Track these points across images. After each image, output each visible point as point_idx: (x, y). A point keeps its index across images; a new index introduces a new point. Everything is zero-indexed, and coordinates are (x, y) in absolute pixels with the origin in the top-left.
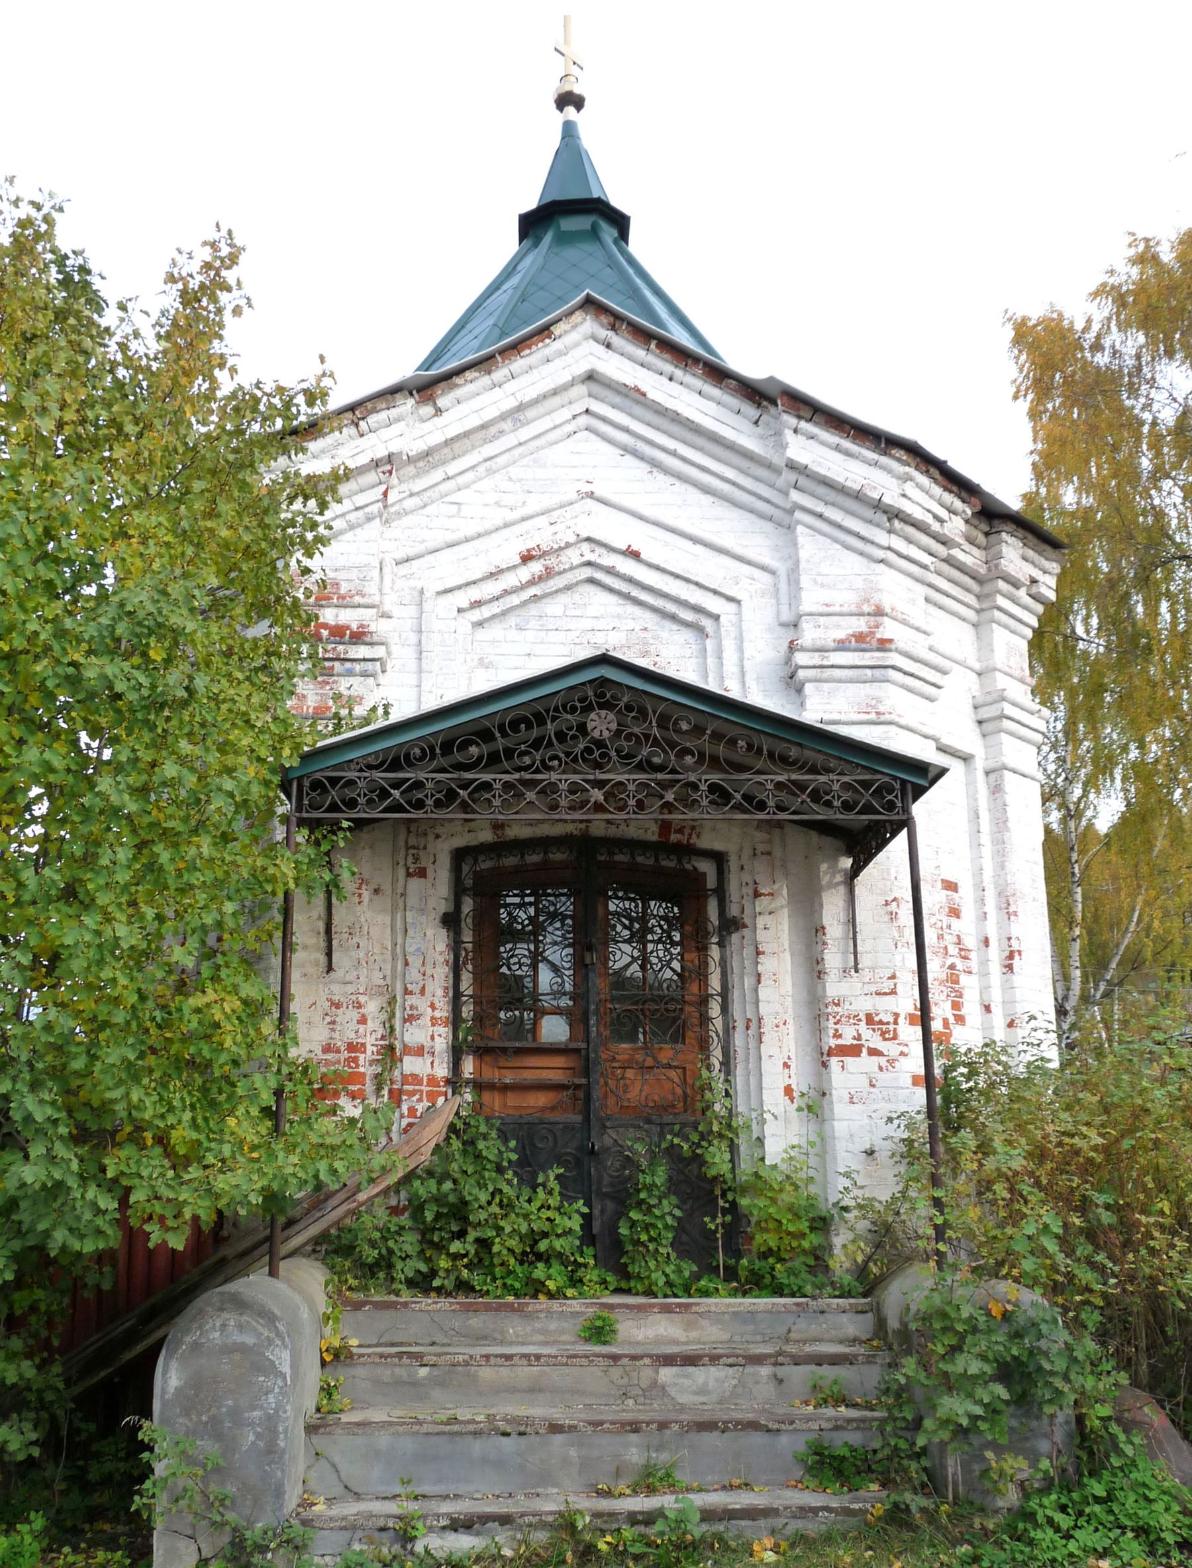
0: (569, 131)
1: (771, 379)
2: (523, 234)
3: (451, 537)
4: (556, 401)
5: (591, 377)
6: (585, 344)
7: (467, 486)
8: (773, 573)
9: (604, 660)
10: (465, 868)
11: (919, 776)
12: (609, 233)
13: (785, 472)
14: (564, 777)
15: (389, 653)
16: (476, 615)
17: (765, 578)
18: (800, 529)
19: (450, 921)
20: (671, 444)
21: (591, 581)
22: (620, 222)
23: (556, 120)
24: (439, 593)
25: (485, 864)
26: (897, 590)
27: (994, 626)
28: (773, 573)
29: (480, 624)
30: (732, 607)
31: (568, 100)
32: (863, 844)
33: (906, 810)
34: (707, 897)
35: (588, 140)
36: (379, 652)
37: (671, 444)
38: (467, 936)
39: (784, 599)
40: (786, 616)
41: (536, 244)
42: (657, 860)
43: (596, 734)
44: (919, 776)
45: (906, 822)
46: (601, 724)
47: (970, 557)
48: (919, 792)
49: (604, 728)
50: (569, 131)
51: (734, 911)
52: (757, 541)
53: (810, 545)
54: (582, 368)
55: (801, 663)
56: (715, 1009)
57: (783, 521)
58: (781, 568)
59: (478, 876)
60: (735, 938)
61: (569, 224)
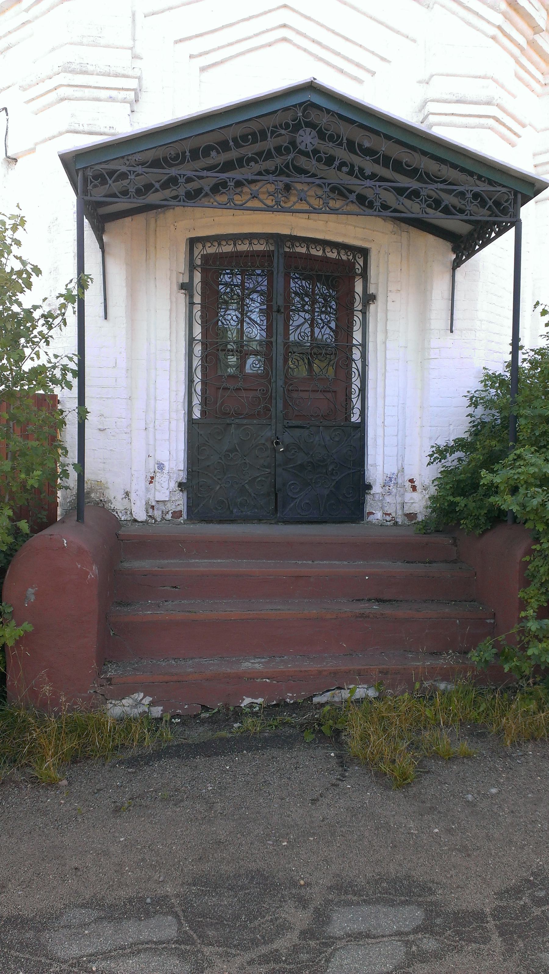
25: (211, 250)
29: (203, 69)
32: (465, 245)
33: (516, 214)
38: (197, 299)
45: (517, 223)
48: (526, 199)
59: (206, 258)
60: (372, 307)
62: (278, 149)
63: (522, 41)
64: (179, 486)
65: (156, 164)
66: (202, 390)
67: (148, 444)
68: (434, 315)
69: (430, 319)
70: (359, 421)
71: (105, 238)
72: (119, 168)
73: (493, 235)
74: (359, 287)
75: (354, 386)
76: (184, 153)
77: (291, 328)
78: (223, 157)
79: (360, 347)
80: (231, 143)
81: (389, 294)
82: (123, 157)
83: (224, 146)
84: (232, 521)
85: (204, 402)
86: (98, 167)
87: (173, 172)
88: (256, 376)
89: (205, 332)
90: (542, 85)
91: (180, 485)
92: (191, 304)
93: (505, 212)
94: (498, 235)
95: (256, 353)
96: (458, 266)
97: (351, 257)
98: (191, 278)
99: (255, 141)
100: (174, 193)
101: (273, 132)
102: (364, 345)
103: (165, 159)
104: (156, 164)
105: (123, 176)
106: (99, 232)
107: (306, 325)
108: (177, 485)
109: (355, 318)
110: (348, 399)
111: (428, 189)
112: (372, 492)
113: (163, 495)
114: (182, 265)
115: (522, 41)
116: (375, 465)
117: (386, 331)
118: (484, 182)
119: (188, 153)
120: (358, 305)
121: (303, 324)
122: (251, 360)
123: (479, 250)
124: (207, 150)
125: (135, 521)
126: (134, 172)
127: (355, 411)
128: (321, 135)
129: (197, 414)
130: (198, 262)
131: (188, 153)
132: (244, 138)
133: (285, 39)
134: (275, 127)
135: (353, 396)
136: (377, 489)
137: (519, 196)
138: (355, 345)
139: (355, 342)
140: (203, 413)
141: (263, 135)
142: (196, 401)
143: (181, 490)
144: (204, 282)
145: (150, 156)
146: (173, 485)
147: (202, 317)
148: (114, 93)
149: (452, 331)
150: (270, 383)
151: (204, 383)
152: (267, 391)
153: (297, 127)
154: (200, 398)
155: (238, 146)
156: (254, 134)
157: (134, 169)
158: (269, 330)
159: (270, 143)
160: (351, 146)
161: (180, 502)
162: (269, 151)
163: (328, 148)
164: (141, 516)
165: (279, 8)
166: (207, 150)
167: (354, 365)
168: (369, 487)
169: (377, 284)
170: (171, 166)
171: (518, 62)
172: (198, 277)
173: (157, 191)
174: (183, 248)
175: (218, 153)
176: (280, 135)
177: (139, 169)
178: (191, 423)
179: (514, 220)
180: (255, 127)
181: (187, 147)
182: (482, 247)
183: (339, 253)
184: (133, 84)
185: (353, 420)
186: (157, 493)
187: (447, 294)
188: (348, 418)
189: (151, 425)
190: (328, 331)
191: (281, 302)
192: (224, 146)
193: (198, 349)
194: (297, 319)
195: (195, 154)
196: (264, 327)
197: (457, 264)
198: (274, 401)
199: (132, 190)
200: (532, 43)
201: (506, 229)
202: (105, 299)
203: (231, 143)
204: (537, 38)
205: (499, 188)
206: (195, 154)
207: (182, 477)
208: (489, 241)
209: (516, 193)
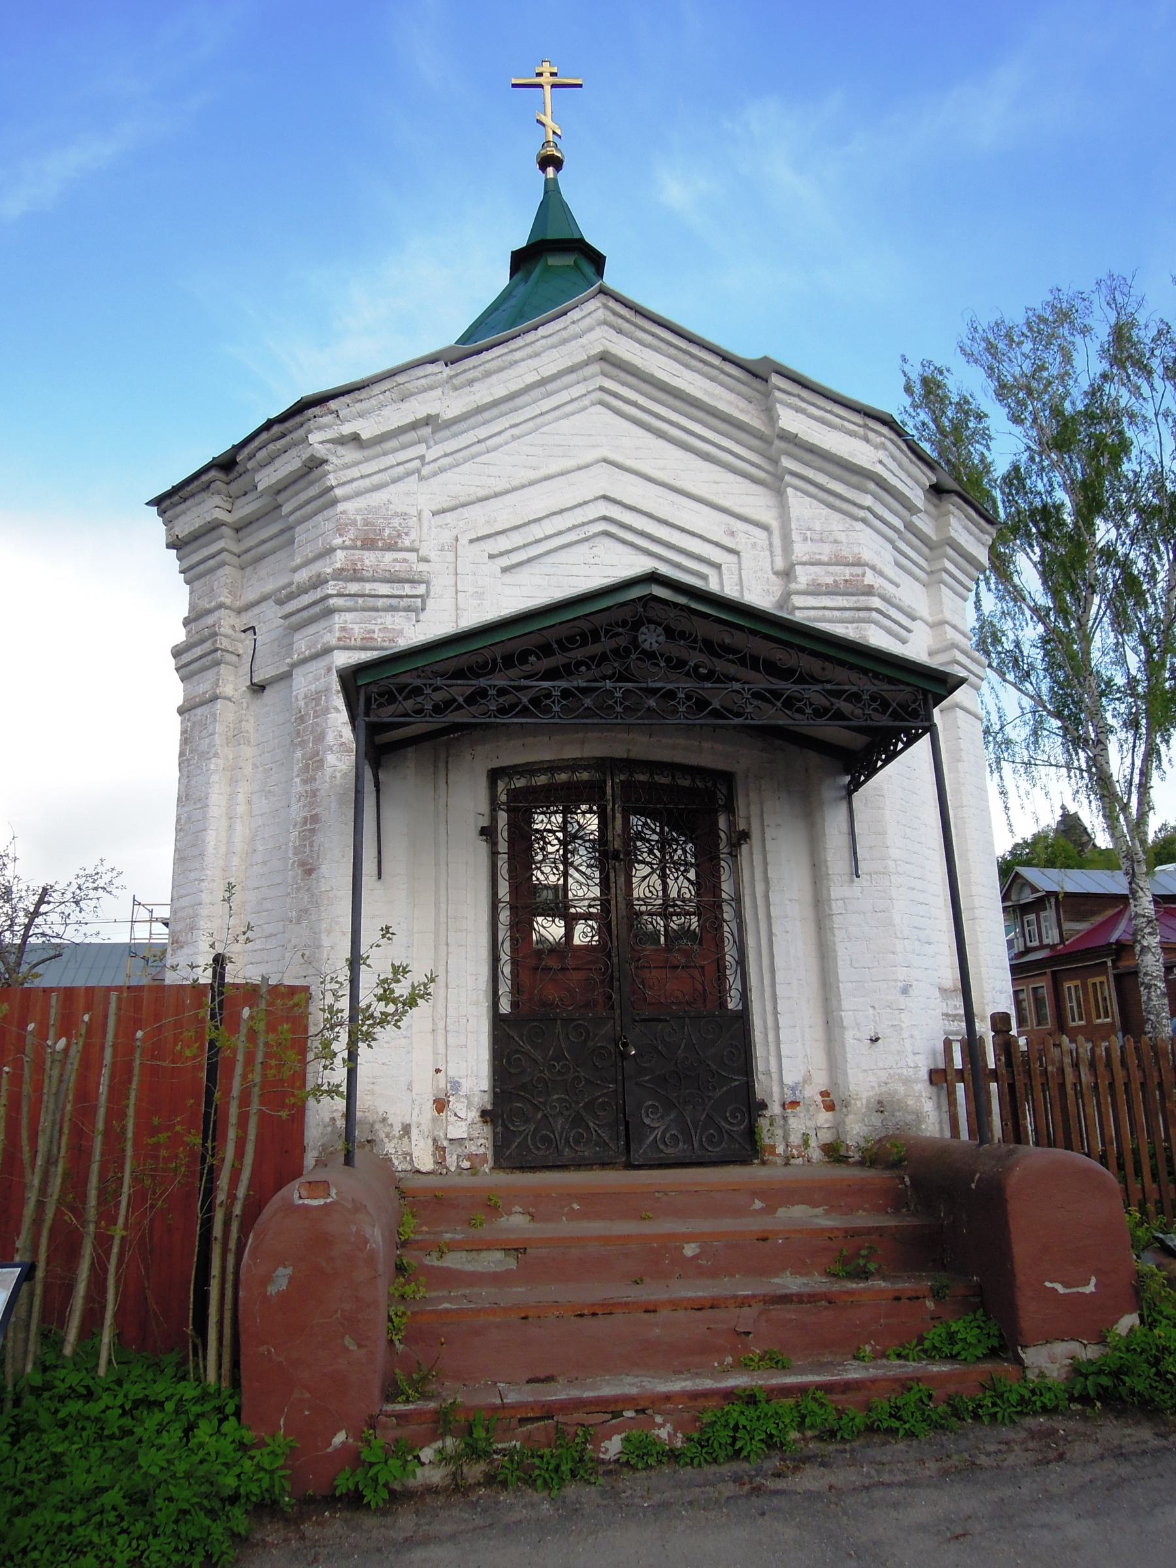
0: (551, 191)
1: (765, 359)
2: (514, 270)
3: (482, 493)
4: (573, 377)
5: (604, 357)
6: (598, 329)
7: (495, 449)
8: (765, 528)
9: (653, 578)
10: (501, 785)
11: (935, 685)
12: (589, 270)
13: (777, 442)
14: (620, 684)
15: (428, 591)
16: (505, 561)
17: (763, 534)
18: (790, 491)
19: (488, 832)
20: (674, 417)
21: (606, 534)
22: (597, 261)
23: (536, 180)
24: (471, 541)
25: (520, 783)
26: (869, 545)
27: (942, 586)
28: (765, 528)
29: (505, 570)
30: (732, 558)
31: (549, 162)
32: (862, 759)
33: (929, 717)
34: (716, 811)
35: (568, 194)
36: (421, 589)
37: (674, 417)
38: (503, 847)
39: (778, 550)
40: (780, 564)
41: (526, 280)
42: (673, 778)
43: (646, 646)
44: (935, 685)
45: (931, 729)
46: (651, 638)
47: (924, 524)
48: (939, 699)
49: (653, 641)
50: (551, 191)
51: (742, 826)
52: (755, 502)
53: (801, 506)
54: (596, 349)
55: (798, 605)
56: (728, 913)
57: (776, 484)
58: (775, 525)
59: (513, 794)
60: (745, 848)
61: (554, 261)
62: (615, 651)
63: (899, 524)
64: (482, 1116)
65: (459, 674)
66: (512, 972)
67: (436, 1054)
68: (830, 856)
69: (826, 861)
70: (740, 1007)
71: (382, 776)
72: (409, 681)
73: (900, 746)
74: (722, 823)
75: (728, 958)
76: (494, 661)
77: (634, 880)
78: (547, 663)
79: (733, 903)
80: (555, 646)
81: (766, 830)
82: (416, 669)
83: (545, 650)
84: (619, 1237)
85: (516, 988)
86: (382, 683)
87: (483, 682)
88: (587, 948)
89: (514, 890)
90: (927, 573)
91: (484, 1114)
92: (494, 854)
93: (914, 714)
94: (907, 745)
95: (587, 917)
96: (856, 790)
97: (710, 784)
98: (494, 819)
99: (584, 643)
100: (482, 708)
101: (607, 632)
102: (738, 899)
103: (470, 669)
104: (459, 674)
105: (417, 691)
106: (376, 767)
107: (655, 877)
108: (478, 1114)
109: (723, 863)
110: (721, 978)
111: (813, 694)
112: (767, 1113)
113: (458, 1130)
114: (484, 806)
115: (899, 524)
116: (768, 1073)
117: (766, 880)
118: (882, 680)
119: (499, 660)
120: (723, 847)
121: (651, 873)
122: (580, 928)
123: (882, 767)
124: (524, 657)
125: (418, 1171)
126: (431, 685)
127: (733, 992)
128: (670, 633)
129: (505, 1007)
130: (503, 798)
131: (499, 660)
132: (571, 639)
133: (606, 534)
134: (610, 625)
135: (728, 972)
136: (775, 1109)
137: (930, 696)
138: (725, 901)
139: (724, 896)
140: (514, 1005)
141: (595, 636)
142: (504, 988)
143: (485, 1122)
144: (511, 825)
145: (452, 666)
146: (474, 1115)
147: (510, 871)
148: (394, 601)
149: (858, 876)
150: (610, 958)
151: (515, 963)
152: (607, 969)
153: (637, 625)
154: (509, 982)
155: (564, 649)
156: (583, 635)
157: (431, 682)
158: (605, 884)
159: (606, 645)
160: (709, 647)
161: (481, 1142)
162: (604, 654)
163: (677, 649)
164: (425, 1162)
165: (597, 499)
166: (524, 657)
167: (726, 928)
168: (763, 1106)
169: (748, 818)
170: (478, 676)
171: (895, 548)
172: (503, 817)
173: (460, 707)
174: (483, 783)
175: (539, 658)
176: (619, 634)
177: (439, 682)
178: (498, 1020)
179: (926, 724)
180: (585, 626)
181: (498, 652)
182: (886, 762)
183: (693, 780)
184: (421, 589)
185: (730, 1006)
186: (450, 1128)
187: (845, 827)
188: (723, 1004)
189: (441, 1025)
190: (686, 884)
191: (617, 844)
192: (545, 650)
193: (504, 916)
194: (641, 870)
195: (508, 661)
196: (597, 881)
197: (856, 785)
198: (616, 984)
199: (429, 707)
200: (909, 526)
201: (918, 737)
202: (379, 852)
203: (555, 646)
204: (914, 519)
205: (902, 687)
206: (508, 661)
207: (486, 1101)
208: (895, 754)
209: (925, 692)
